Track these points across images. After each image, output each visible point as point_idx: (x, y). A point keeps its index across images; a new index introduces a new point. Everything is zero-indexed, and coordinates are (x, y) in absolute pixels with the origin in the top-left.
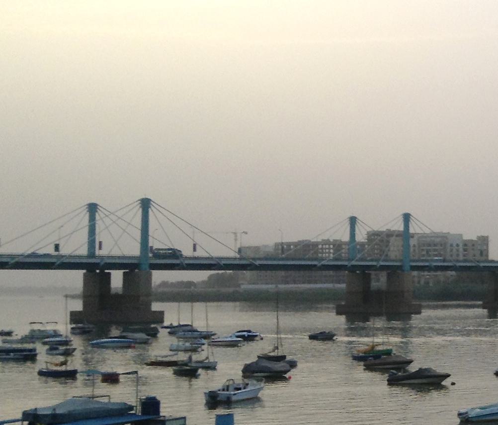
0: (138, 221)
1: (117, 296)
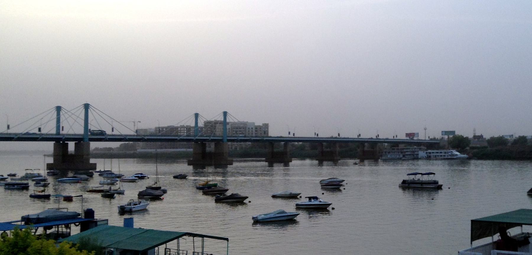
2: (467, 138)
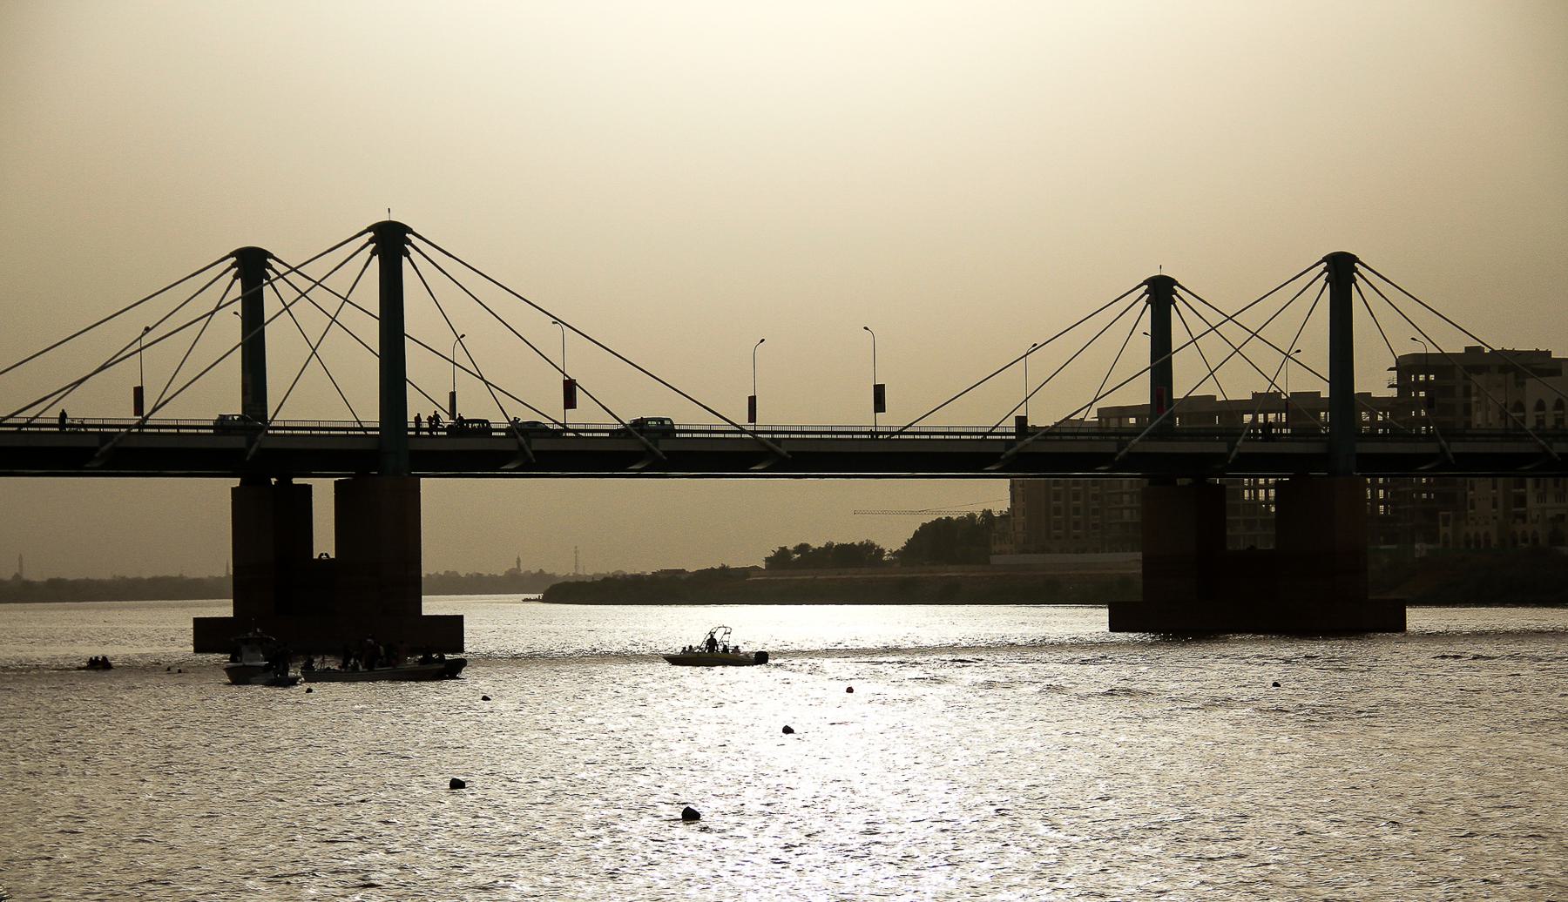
0: (370, 293)
1: (324, 563)
2: (219, 578)
